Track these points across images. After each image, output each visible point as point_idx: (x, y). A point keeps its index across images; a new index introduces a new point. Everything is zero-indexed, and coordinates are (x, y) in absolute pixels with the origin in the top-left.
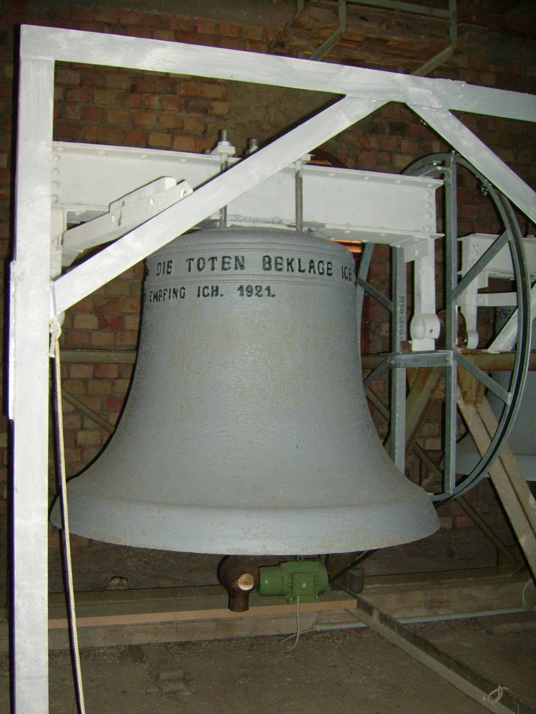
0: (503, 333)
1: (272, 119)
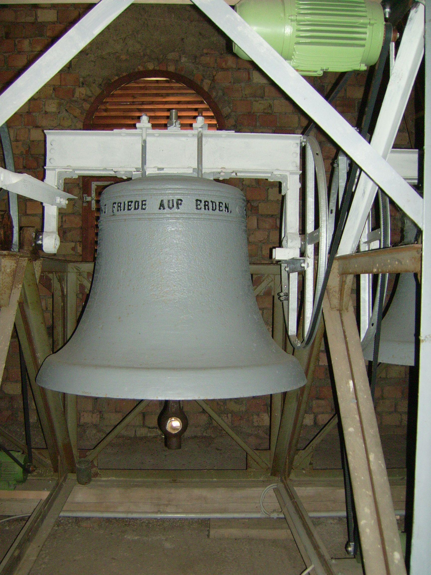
0: (410, 21)
1: (130, 49)
